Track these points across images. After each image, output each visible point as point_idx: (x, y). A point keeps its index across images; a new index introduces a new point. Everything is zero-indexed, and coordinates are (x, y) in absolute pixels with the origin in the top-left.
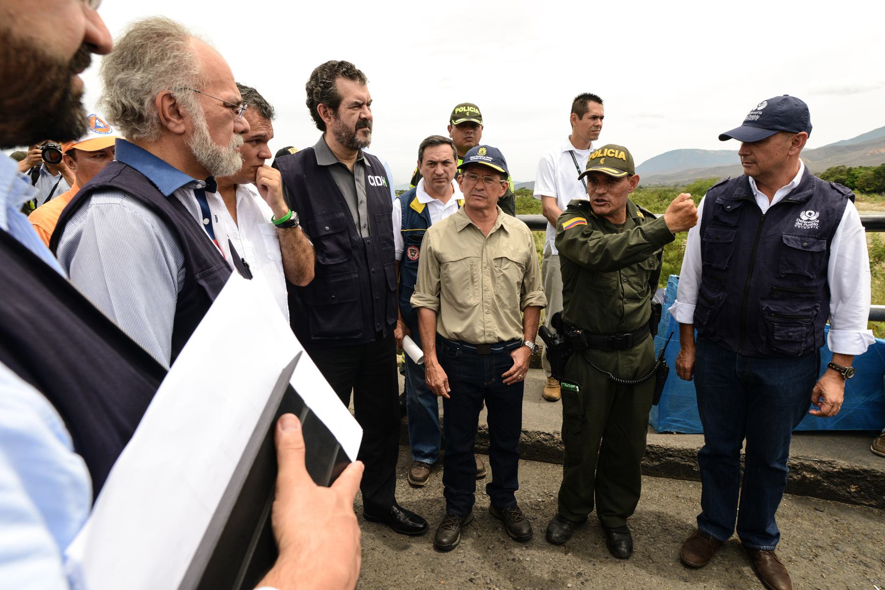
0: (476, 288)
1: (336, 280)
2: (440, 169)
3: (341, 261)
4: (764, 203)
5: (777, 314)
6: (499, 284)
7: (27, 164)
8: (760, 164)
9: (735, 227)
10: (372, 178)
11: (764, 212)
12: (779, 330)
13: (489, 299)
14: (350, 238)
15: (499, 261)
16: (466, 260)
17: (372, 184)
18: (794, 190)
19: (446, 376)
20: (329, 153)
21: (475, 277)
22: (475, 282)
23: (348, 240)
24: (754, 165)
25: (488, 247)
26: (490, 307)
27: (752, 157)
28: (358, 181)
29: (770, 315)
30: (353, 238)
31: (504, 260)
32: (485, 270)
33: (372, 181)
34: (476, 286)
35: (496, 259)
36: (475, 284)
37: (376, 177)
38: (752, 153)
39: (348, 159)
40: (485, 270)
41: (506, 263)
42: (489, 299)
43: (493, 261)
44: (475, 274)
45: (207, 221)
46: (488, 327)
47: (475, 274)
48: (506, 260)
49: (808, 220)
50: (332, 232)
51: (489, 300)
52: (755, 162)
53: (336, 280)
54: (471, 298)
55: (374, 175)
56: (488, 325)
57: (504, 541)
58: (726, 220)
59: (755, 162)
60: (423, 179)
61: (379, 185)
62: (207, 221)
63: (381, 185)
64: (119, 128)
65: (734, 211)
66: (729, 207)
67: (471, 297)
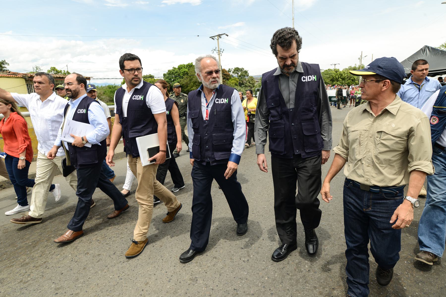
0: (362, 149)
1: (275, 127)
2: (214, 75)
3: (277, 119)
6: (378, 148)
7: (412, 152)
13: (370, 157)
15: (380, 133)
19: (254, 133)
21: (361, 142)
22: (362, 145)
25: (375, 124)
26: (370, 163)
31: (383, 132)
32: (370, 139)
34: (362, 148)
35: (378, 132)
36: (362, 147)
40: (370, 139)
41: (384, 136)
42: (370, 157)
43: (376, 133)
44: (362, 141)
46: (367, 175)
47: (362, 141)
48: (385, 133)
50: (274, 106)
51: (369, 158)
53: (275, 127)
54: (358, 155)
56: (366, 174)
57: (325, 255)
64: (290, 50)
67: (357, 154)
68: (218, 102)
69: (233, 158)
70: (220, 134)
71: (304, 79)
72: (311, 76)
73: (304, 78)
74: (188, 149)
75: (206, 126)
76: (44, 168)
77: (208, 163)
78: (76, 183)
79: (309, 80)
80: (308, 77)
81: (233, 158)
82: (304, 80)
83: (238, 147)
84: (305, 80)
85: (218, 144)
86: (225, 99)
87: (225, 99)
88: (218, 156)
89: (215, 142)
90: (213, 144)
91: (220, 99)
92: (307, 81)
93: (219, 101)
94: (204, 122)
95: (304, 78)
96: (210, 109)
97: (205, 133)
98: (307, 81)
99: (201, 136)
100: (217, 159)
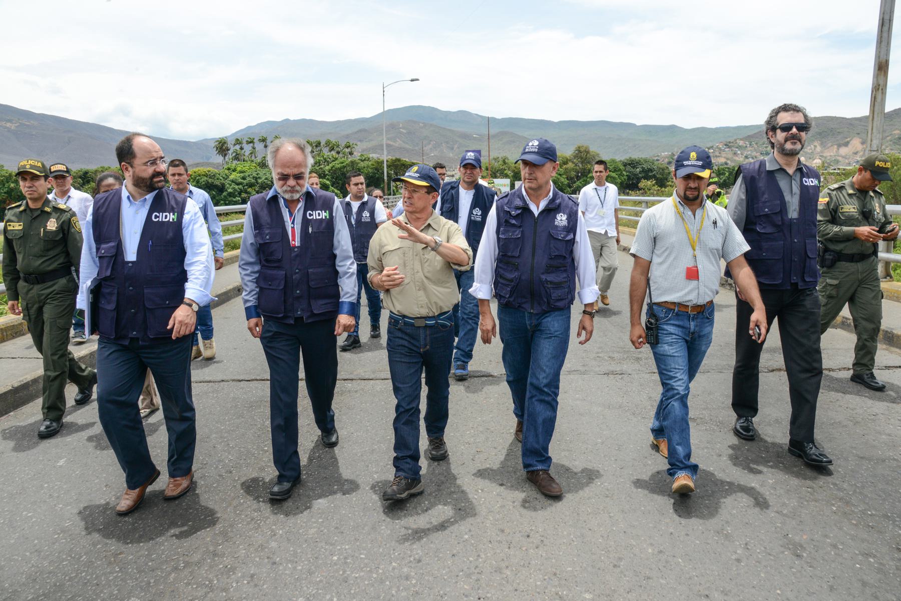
4: (536, 210)
5: (551, 282)
8: (539, 181)
9: (520, 227)
10: (807, 180)
11: (536, 216)
12: (554, 293)
14: (782, 218)
16: (401, 249)
17: (806, 184)
18: (550, 200)
20: (775, 162)
21: (406, 262)
23: (780, 219)
24: (535, 181)
27: (534, 175)
28: (795, 180)
29: (547, 284)
30: (785, 218)
33: (806, 182)
36: (407, 268)
37: (810, 180)
38: (534, 172)
39: (789, 165)
45: (292, 226)
49: (561, 220)
52: (536, 179)
55: (809, 178)
58: (514, 222)
59: (536, 179)
60: (350, 195)
61: (811, 184)
62: (292, 226)
63: (814, 184)
65: (515, 217)
66: (513, 213)
68: (158, 219)
69: (346, 308)
70: (319, 270)
71: (310, 215)
72: (167, 214)
73: (310, 213)
74: (633, 259)
75: (297, 256)
76: (194, 293)
77: (299, 320)
78: (437, 312)
79: (164, 220)
80: (164, 214)
81: (346, 308)
82: (155, 218)
83: (602, 269)
84: (312, 217)
85: (318, 286)
86: (171, 214)
87: (171, 214)
88: (319, 307)
89: (313, 283)
90: (309, 287)
91: (161, 214)
92: (315, 218)
93: (159, 217)
94: (292, 249)
95: (310, 213)
96: (299, 226)
97: (295, 268)
98: (160, 220)
99: (286, 274)
100: (315, 312)
